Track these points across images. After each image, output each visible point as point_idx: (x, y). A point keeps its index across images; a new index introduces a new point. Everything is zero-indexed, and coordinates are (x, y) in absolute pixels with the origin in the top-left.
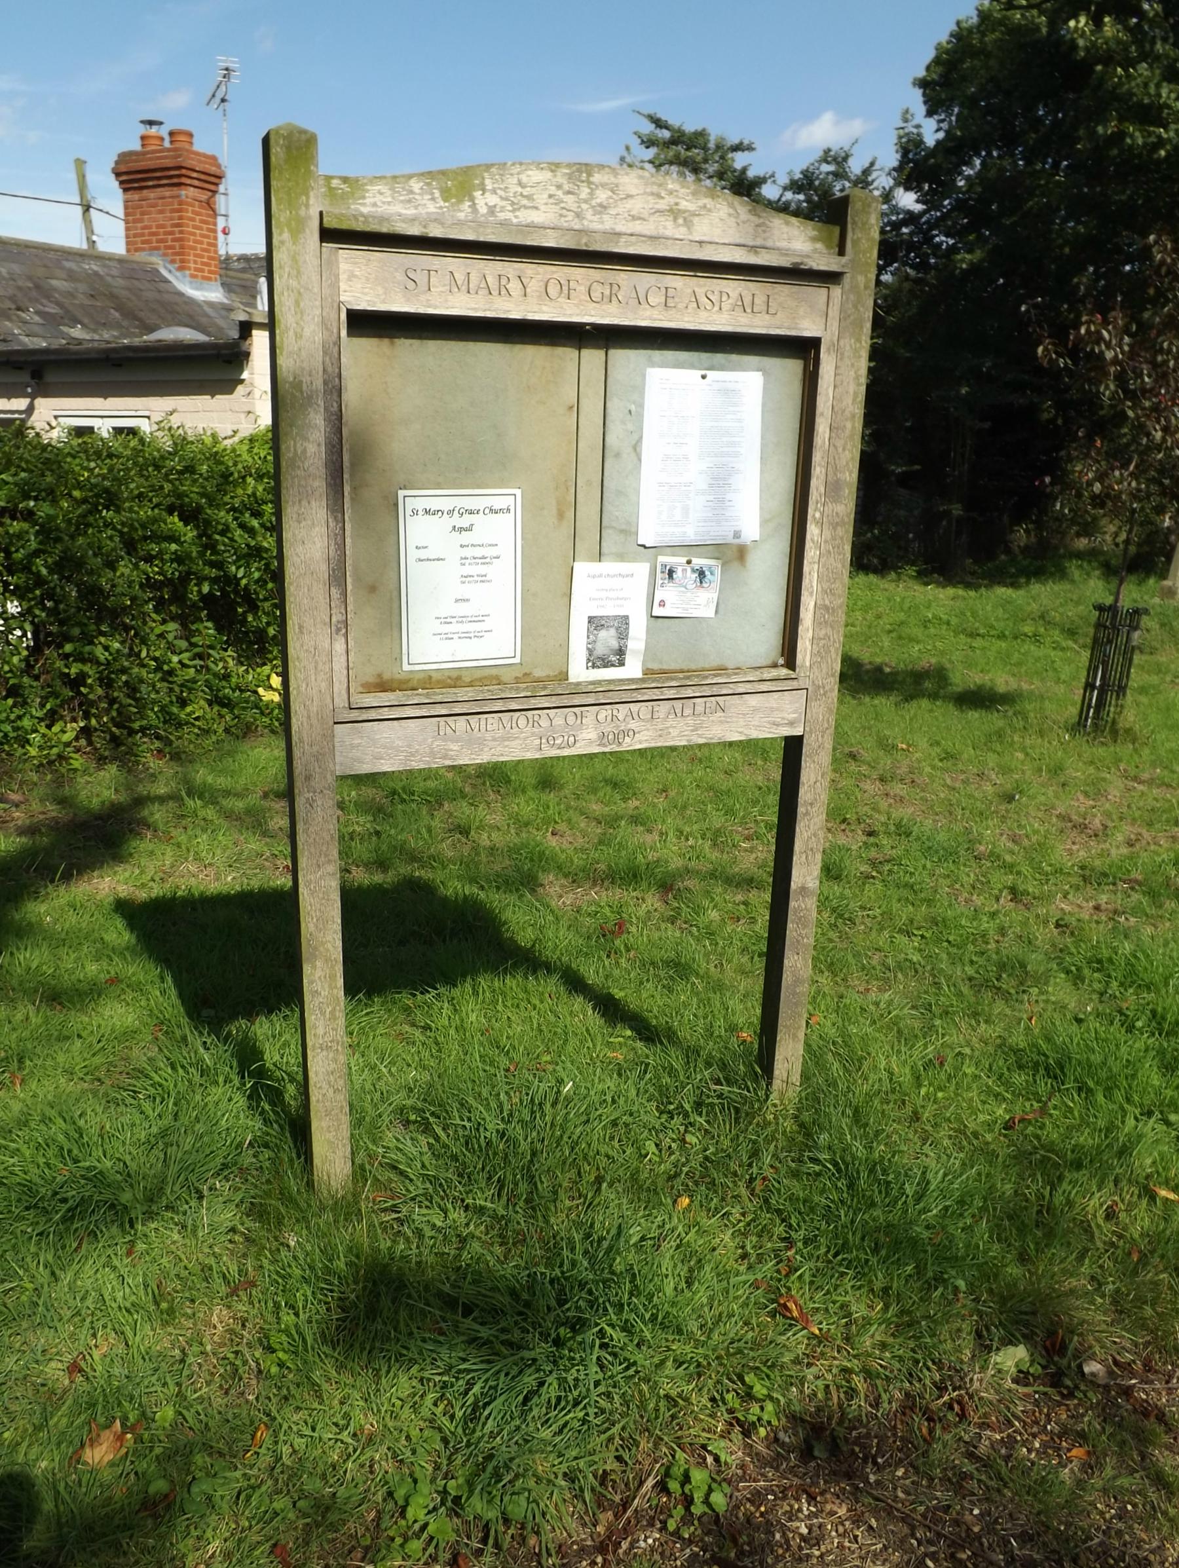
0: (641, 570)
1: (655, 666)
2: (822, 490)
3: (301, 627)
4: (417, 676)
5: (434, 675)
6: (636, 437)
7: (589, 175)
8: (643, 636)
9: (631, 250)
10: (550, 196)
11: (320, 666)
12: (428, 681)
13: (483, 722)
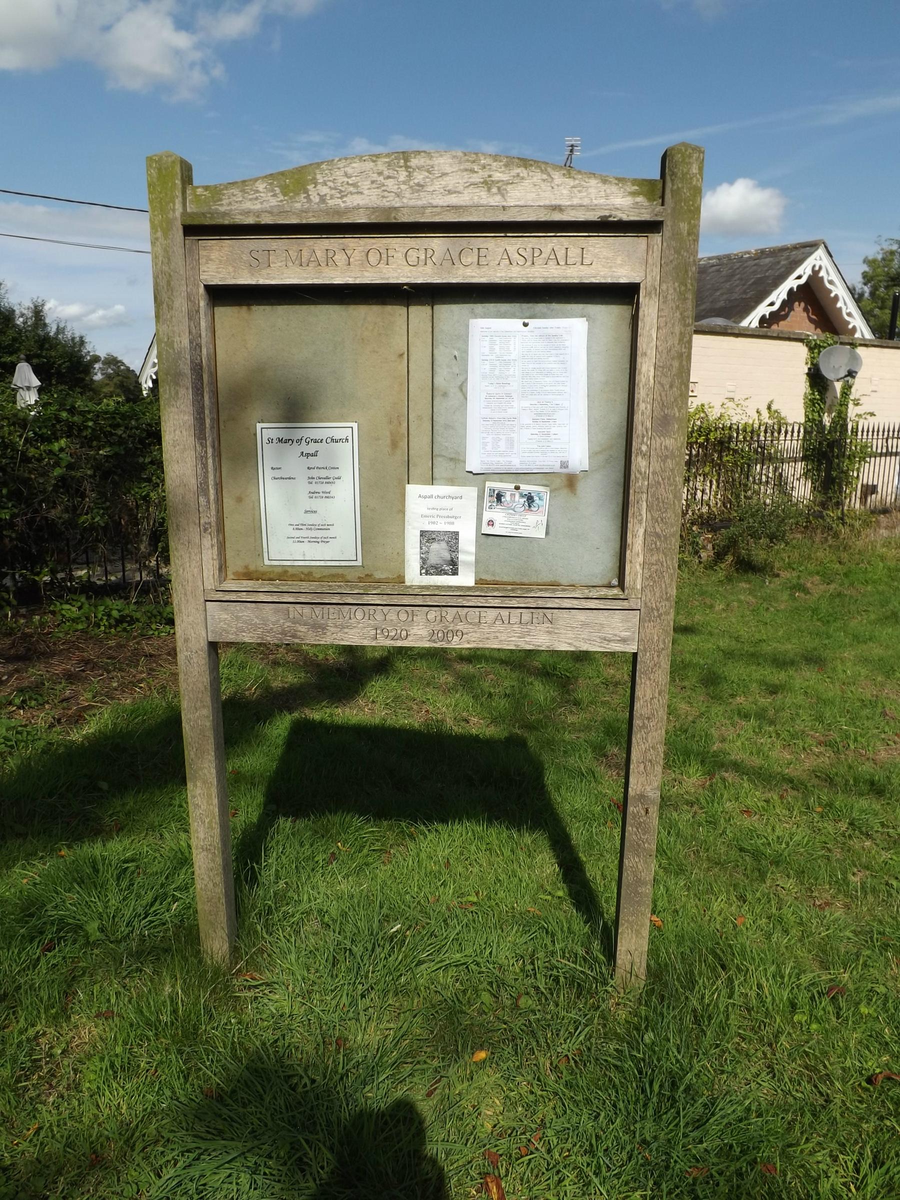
0: (471, 492)
1: (488, 577)
2: (649, 425)
3: (177, 526)
4: (276, 570)
5: (289, 569)
6: (461, 378)
7: (406, 160)
8: (472, 549)
9: (437, 219)
10: (373, 182)
11: (193, 557)
12: (284, 574)
13: (325, 610)
